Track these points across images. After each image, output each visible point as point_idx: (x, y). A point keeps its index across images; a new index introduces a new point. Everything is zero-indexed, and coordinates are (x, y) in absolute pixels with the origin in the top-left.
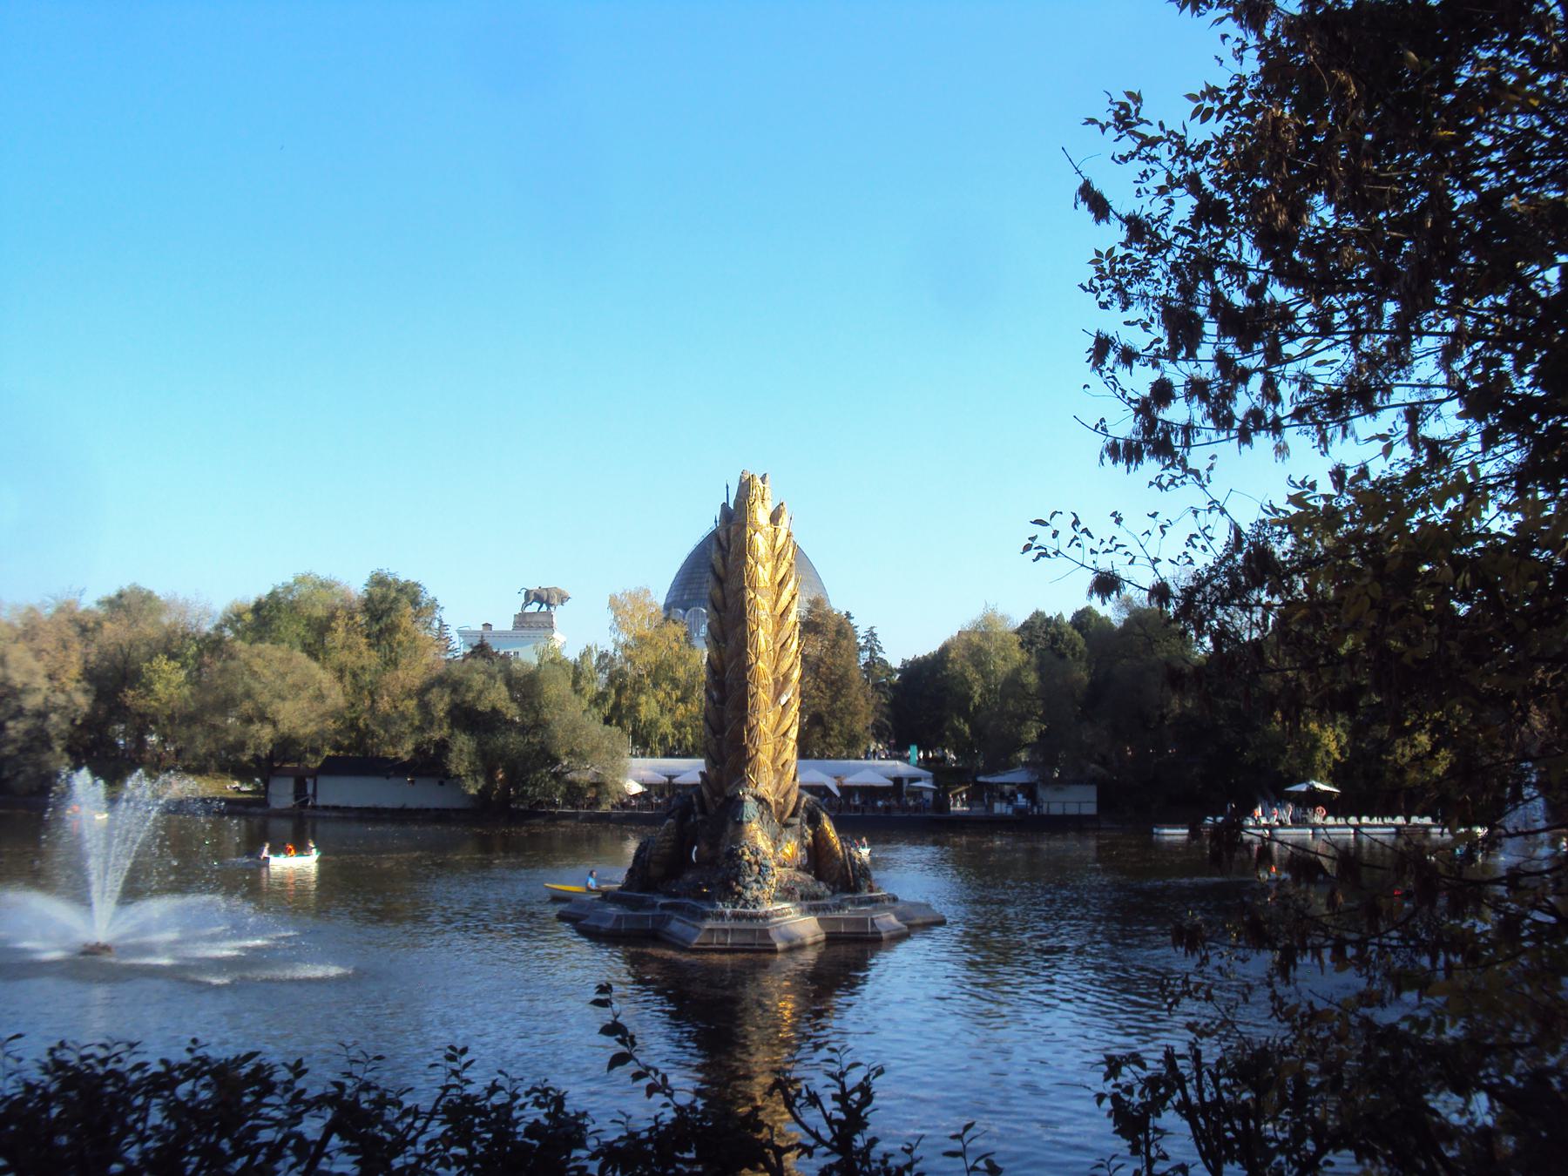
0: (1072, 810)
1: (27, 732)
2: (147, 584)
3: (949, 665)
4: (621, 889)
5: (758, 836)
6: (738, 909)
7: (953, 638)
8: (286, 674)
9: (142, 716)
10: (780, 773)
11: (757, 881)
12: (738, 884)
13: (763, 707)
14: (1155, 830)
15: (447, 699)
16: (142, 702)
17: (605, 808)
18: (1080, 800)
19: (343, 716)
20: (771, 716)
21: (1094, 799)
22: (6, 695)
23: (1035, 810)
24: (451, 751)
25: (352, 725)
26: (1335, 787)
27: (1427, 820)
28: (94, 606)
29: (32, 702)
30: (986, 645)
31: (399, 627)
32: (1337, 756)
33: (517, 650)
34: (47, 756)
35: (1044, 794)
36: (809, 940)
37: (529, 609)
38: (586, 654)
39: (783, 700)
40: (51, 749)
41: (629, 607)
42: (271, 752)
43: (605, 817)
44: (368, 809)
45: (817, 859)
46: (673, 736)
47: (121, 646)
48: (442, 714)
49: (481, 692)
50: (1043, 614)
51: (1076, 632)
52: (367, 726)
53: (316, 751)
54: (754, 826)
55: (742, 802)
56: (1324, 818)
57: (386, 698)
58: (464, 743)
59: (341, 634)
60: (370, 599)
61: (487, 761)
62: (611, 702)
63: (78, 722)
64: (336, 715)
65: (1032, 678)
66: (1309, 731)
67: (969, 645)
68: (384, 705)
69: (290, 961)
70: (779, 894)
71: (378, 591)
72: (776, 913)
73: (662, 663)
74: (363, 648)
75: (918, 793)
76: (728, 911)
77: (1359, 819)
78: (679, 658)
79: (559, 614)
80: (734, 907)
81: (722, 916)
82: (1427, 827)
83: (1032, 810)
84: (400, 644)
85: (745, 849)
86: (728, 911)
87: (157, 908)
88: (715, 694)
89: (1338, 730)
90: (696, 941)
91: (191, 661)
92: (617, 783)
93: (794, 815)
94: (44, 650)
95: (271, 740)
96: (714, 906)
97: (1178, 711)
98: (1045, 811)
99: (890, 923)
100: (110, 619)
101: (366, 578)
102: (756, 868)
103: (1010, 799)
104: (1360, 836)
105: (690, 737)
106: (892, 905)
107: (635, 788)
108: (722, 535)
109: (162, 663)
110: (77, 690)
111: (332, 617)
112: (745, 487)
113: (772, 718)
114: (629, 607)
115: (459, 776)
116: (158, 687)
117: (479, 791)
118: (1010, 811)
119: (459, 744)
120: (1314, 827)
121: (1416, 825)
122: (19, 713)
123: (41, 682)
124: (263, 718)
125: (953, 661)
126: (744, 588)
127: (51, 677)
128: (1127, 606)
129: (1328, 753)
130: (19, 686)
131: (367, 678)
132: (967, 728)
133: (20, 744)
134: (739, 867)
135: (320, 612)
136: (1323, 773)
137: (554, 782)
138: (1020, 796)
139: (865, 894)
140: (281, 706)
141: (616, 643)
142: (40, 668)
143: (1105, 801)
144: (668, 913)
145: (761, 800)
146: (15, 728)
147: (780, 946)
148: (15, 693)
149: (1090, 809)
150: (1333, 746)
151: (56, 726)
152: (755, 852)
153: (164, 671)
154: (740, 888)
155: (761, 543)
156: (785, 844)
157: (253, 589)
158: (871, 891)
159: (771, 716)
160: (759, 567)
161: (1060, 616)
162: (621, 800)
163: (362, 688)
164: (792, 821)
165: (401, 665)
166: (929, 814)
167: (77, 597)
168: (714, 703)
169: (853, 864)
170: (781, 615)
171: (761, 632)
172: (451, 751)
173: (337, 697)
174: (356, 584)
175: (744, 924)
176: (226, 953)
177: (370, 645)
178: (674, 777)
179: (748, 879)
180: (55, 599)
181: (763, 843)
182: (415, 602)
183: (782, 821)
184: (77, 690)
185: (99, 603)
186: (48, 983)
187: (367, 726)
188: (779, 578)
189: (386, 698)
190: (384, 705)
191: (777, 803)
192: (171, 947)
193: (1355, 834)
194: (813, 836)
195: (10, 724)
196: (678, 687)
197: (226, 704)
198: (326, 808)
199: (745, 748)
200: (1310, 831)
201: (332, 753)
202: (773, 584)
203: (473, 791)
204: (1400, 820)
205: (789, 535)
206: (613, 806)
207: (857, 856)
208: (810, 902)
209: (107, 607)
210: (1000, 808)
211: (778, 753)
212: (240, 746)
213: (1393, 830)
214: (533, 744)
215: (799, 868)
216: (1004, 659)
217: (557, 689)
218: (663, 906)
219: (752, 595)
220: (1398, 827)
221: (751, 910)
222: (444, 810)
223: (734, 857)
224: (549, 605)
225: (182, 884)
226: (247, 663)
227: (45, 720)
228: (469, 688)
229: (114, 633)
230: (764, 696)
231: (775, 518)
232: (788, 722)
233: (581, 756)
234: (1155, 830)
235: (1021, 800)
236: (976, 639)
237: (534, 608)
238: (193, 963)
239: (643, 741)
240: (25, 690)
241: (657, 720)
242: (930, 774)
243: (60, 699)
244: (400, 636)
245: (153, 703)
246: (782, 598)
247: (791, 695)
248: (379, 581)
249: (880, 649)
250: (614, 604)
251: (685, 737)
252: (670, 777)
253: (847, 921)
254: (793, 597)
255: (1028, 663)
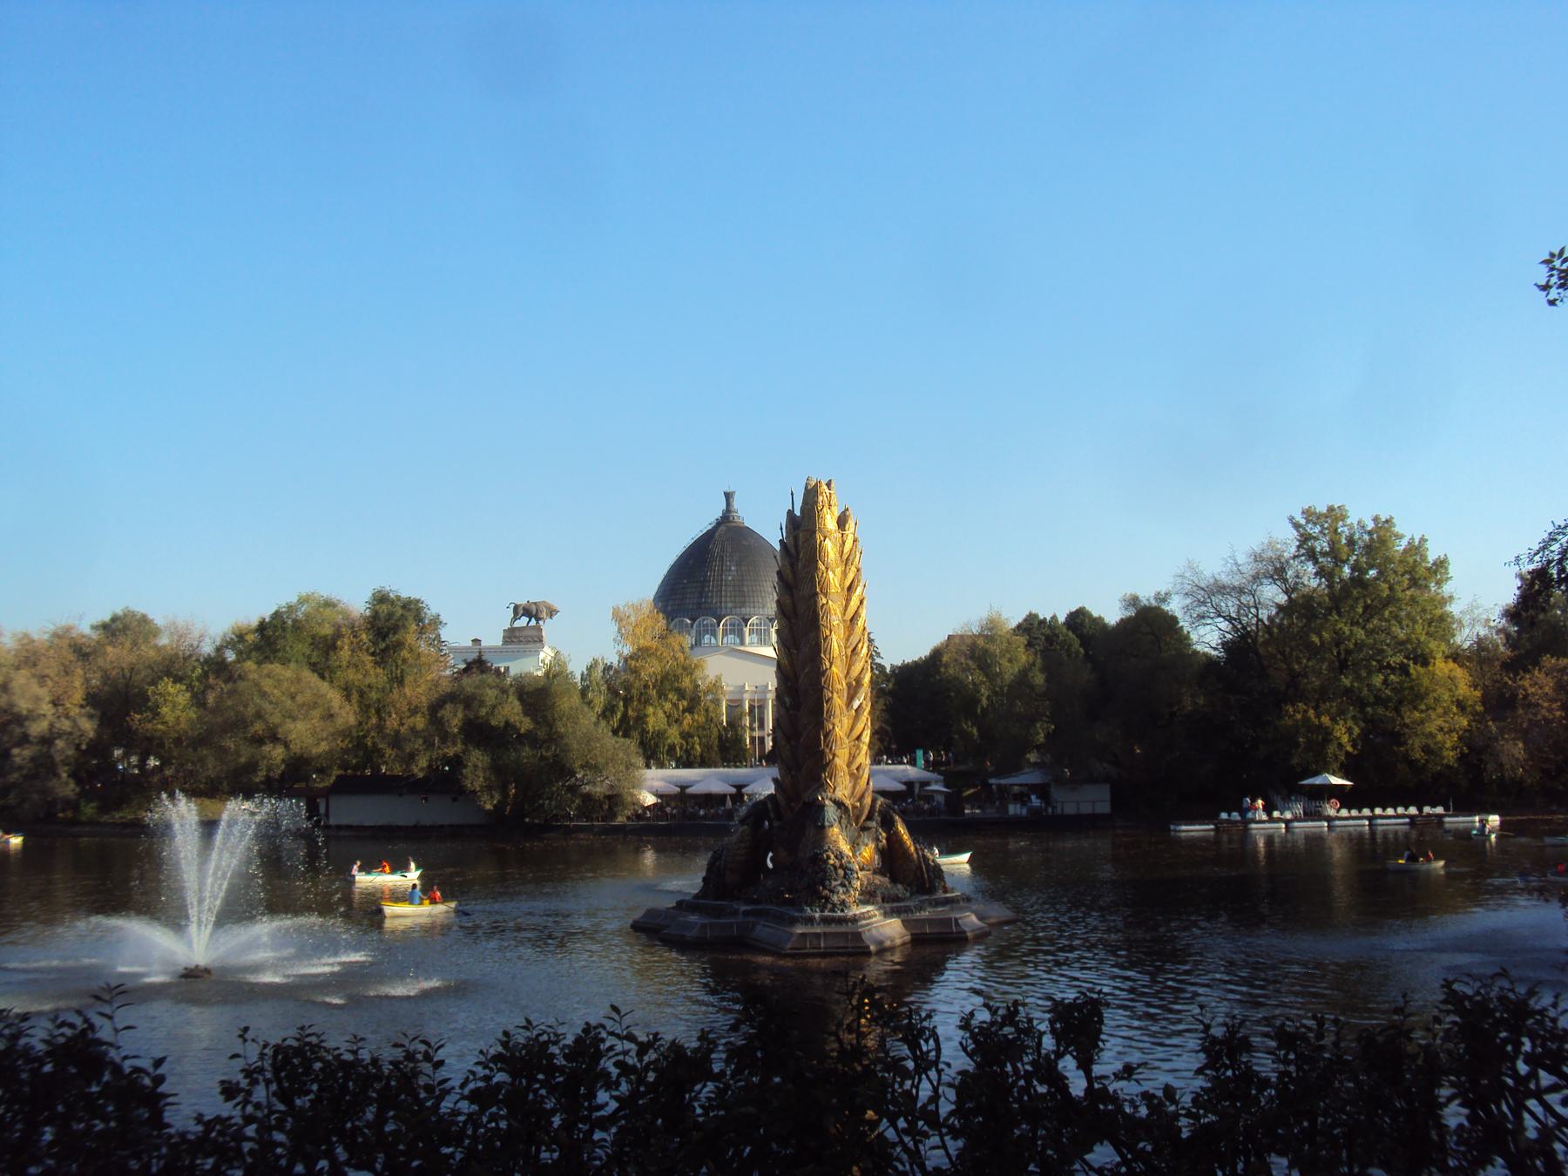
0: (1086, 809)
1: (33, 759)
2: (140, 608)
3: (942, 670)
4: (696, 896)
5: (839, 838)
6: (826, 913)
7: (942, 644)
8: (296, 693)
9: (150, 739)
10: (855, 777)
11: (843, 885)
12: (825, 888)
13: (838, 712)
14: (1172, 827)
15: (460, 715)
16: (149, 726)
17: (620, 820)
18: (1094, 800)
19: (350, 734)
20: (845, 720)
21: (1108, 797)
22: (10, 722)
23: (1050, 810)
24: (466, 767)
25: (359, 744)
26: (1348, 779)
27: (1439, 810)
28: (87, 630)
29: (37, 728)
30: (992, 647)
31: (403, 644)
32: (1349, 749)
33: (507, 664)
34: (53, 783)
35: (1057, 794)
36: (898, 942)
37: (518, 624)
38: (590, 668)
39: (856, 704)
40: (56, 775)
41: (633, 619)
42: (283, 773)
43: (621, 829)
44: (381, 827)
45: (892, 860)
46: (681, 748)
47: (123, 669)
48: (456, 730)
49: (494, 707)
50: (1036, 616)
51: (1070, 633)
52: (374, 744)
53: (321, 771)
54: (836, 830)
55: (822, 807)
56: (1338, 811)
57: (394, 716)
58: (478, 759)
59: (345, 654)
60: (375, 615)
61: (500, 773)
62: (619, 715)
63: (84, 747)
64: (345, 733)
65: (1039, 679)
66: (1321, 724)
67: (973, 647)
68: (392, 723)
69: (382, 979)
70: (862, 898)
71: (384, 609)
72: (863, 916)
73: (667, 674)
74: (369, 666)
75: (929, 798)
76: (817, 915)
77: (1372, 811)
78: (685, 669)
79: (548, 627)
80: (822, 911)
81: (810, 920)
82: (1440, 816)
83: (1046, 810)
84: (404, 661)
85: (830, 853)
86: (817, 915)
87: (265, 928)
88: (787, 700)
89: (1350, 723)
90: (789, 946)
91: (197, 684)
92: (632, 795)
93: (870, 817)
94: (48, 676)
95: (283, 761)
96: (802, 910)
97: (1190, 708)
98: (1059, 811)
99: (972, 922)
100: (111, 643)
101: (368, 596)
102: (841, 872)
103: (1022, 798)
104: (1374, 828)
105: (698, 747)
106: (966, 905)
107: (650, 800)
108: (790, 543)
109: (169, 687)
110: (81, 715)
111: (338, 635)
112: (811, 494)
113: (847, 722)
114: (633, 619)
115: (474, 792)
116: (164, 710)
117: (495, 806)
118: (1024, 812)
119: (473, 759)
120: (1329, 819)
121: (1429, 815)
122: (24, 740)
123: (46, 708)
124: (274, 737)
125: (946, 666)
126: (817, 594)
127: (55, 703)
128: (1134, 605)
129: (1340, 746)
130: (25, 712)
131: (374, 695)
132: (975, 731)
133: (25, 772)
134: (824, 871)
135: (327, 630)
136: (1335, 766)
137: (569, 795)
138: (1033, 797)
139: (940, 895)
140: (292, 726)
141: (620, 655)
142: (43, 692)
143: (1119, 800)
144: (752, 919)
145: (839, 804)
146: (21, 755)
147: (872, 948)
148: (19, 719)
149: (1104, 808)
150: (1345, 739)
151: (62, 751)
152: (840, 856)
153: (169, 694)
154: (826, 892)
155: (830, 548)
156: (863, 848)
157: (254, 609)
158: (946, 891)
159: (845, 720)
160: (830, 573)
161: (1054, 618)
162: (636, 811)
163: (368, 706)
164: (869, 824)
165: (409, 679)
166: (943, 817)
167: (77, 622)
168: (787, 710)
169: (928, 865)
170: (852, 620)
171: (834, 637)
172: (466, 767)
173: (347, 715)
174: (358, 603)
175: (833, 929)
176: (327, 969)
177: (376, 663)
178: (688, 787)
179: (834, 883)
180: (54, 625)
181: (845, 848)
182: (419, 618)
183: (858, 822)
184: (81, 715)
185: (94, 628)
186: (159, 1009)
187: (374, 744)
188: (847, 583)
189: (394, 716)
190: (392, 723)
191: (854, 807)
192: (275, 966)
193: (1370, 825)
194: (887, 839)
195: (16, 751)
196: (684, 698)
197: (238, 724)
198: (339, 827)
199: (823, 753)
200: (1326, 824)
201: (340, 772)
202: (842, 589)
203: (488, 807)
204: (1413, 810)
205: (855, 541)
206: (628, 818)
207: (931, 857)
208: (892, 905)
209: (102, 632)
210: (1014, 809)
211: (852, 757)
212: (252, 767)
213: (1407, 820)
214: (547, 758)
215: (875, 872)
216: (1010, 661)
217: (567, 703)
218: (746, 913)
219: (824, 601)
220: (1411, 817)
221: (839, 914)
222: (458, 826)
223: (818, 861)
224: (538, 619)
225: (276, 905)
226: (257, 685)
227: (49, 748)
228: (482, 704)
229: (117, 655)
230: (838, 701)
231: (842, 522)
232: (860, 726)
233: (596, 769)
234: (1172, 827)
235: (1035, 801)
236: (981, 642)
237: (523, 622)
238: (1460, 910)
239: (653, 752)
240: (32, 716)
241: (665, 731)
242: (942, 777)
243: (66, 725)
244: (405, 653)
245: (160, 727)
246: (852, 603)
247: (863, 699)
248: (381, 598)
249: (878, 654)
250: (618, 617)
251: (693, 748)
252: (683, 788)
253: (930, 922)
254: (861, 602)
255: (1034, 664)
